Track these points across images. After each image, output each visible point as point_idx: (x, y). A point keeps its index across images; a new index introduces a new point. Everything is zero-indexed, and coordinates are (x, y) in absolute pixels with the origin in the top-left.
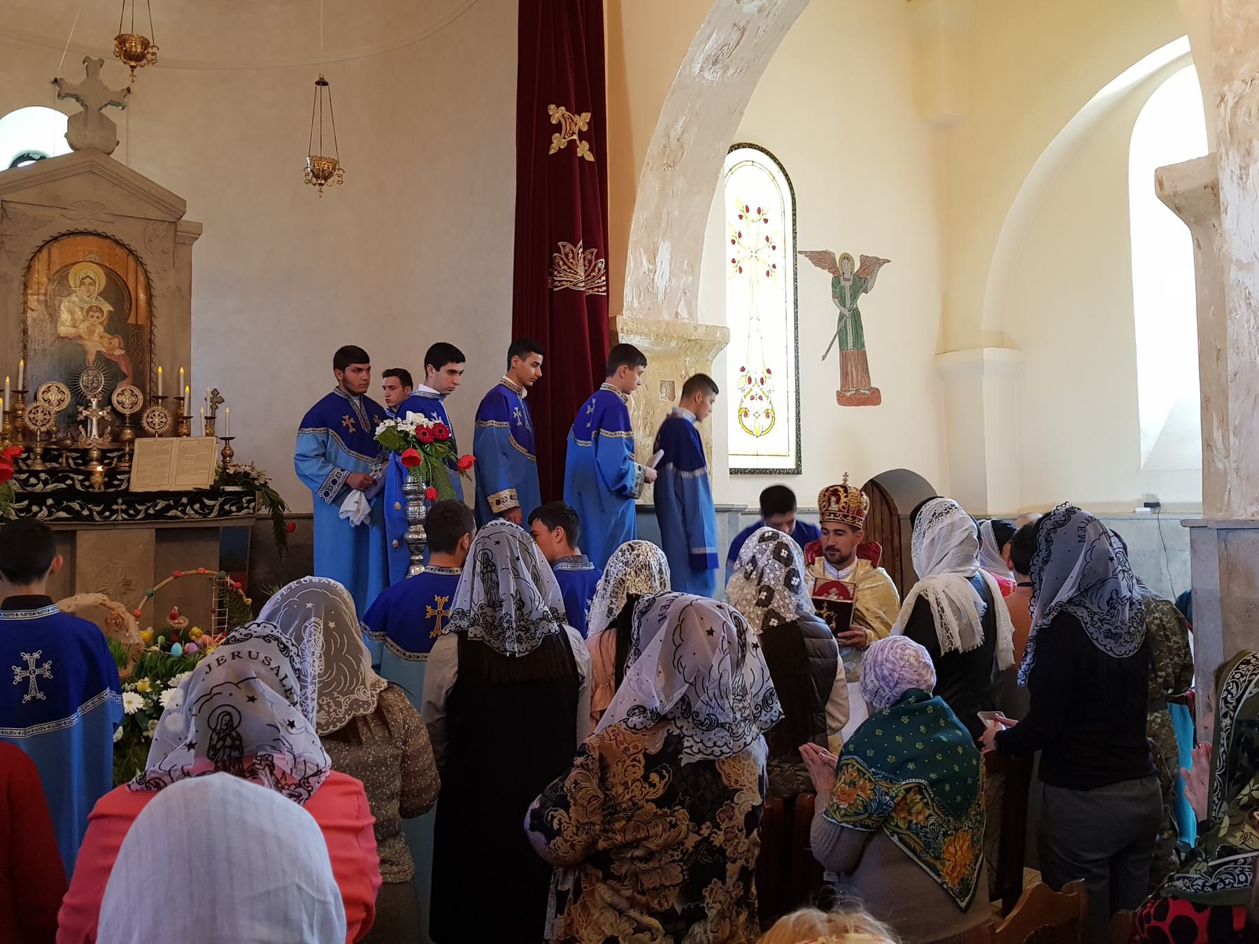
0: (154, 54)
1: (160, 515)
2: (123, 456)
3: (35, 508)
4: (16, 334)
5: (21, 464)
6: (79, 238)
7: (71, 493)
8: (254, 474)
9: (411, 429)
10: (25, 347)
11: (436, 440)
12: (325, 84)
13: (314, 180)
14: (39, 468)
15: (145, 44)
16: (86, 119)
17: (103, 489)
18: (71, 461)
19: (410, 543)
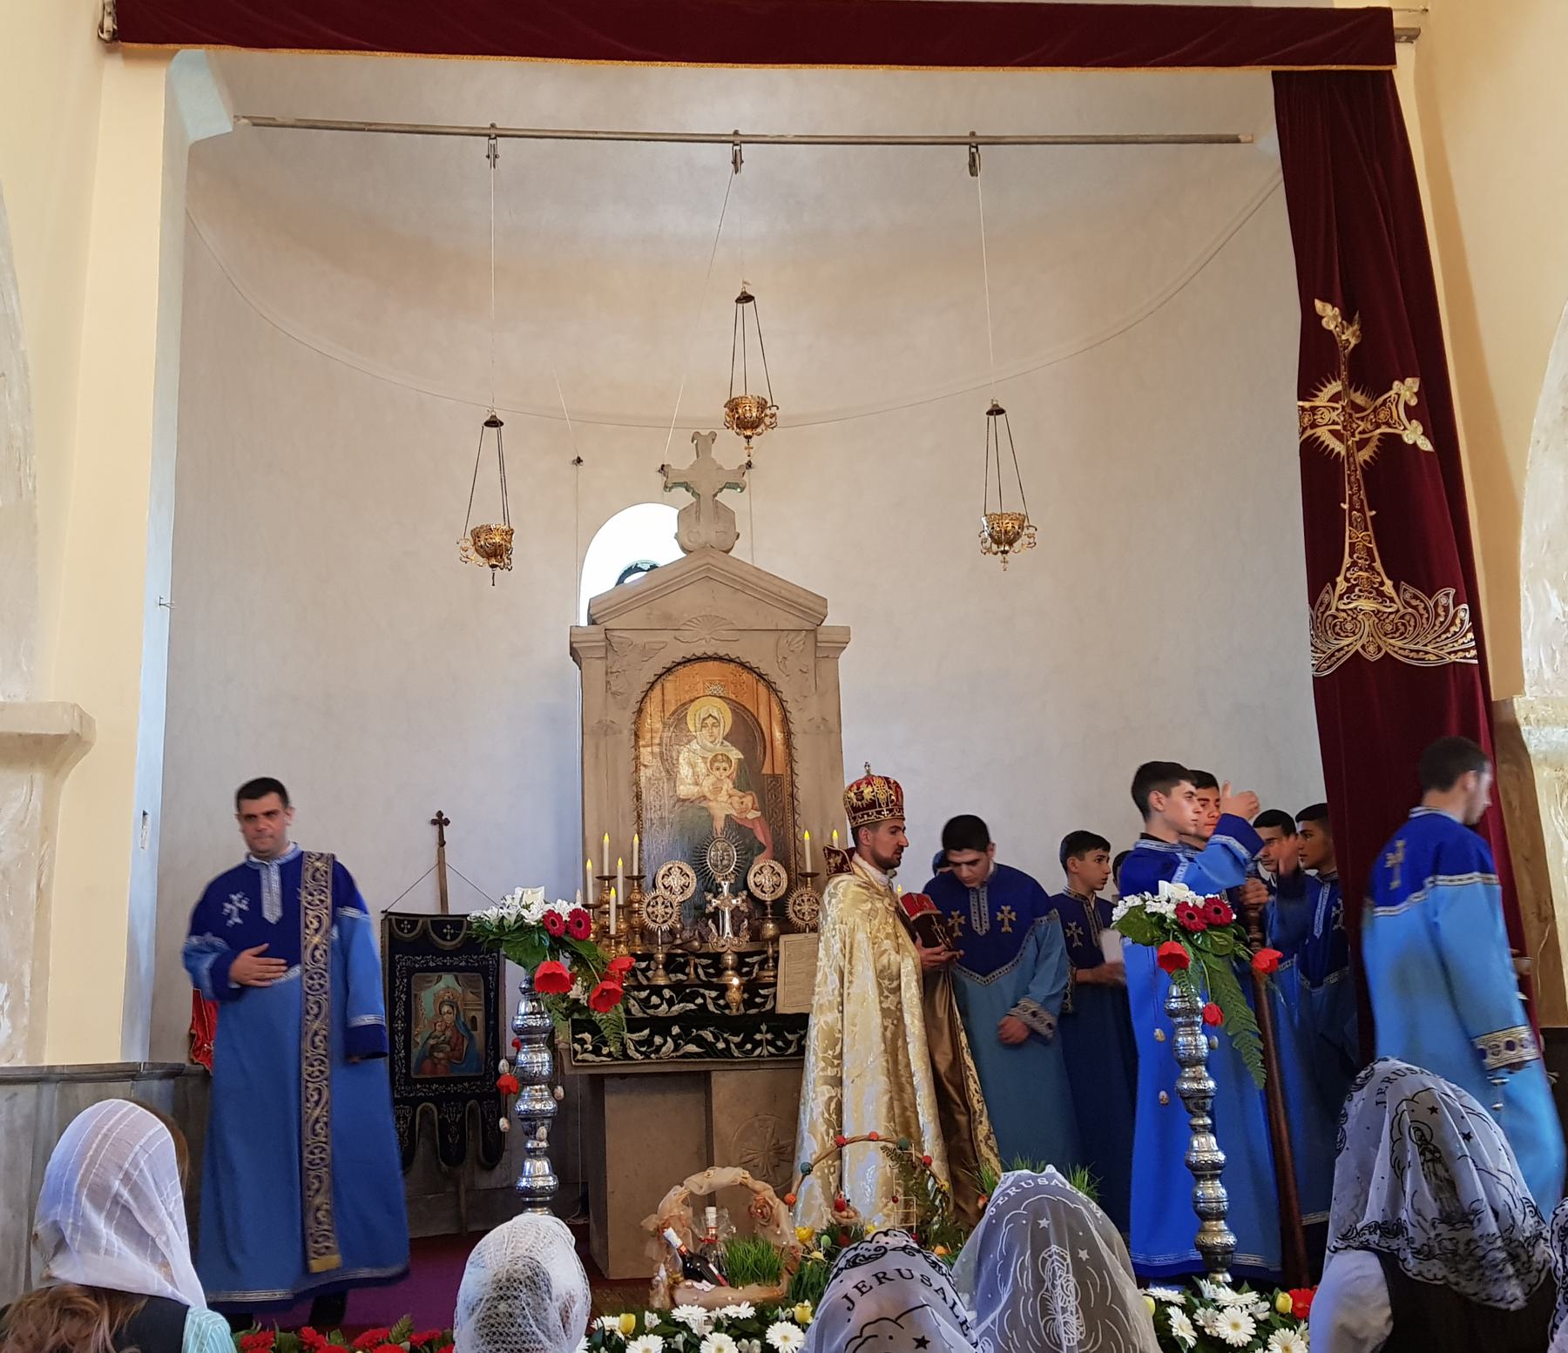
0: (773, 416)
2: (765, 961)
3: (658, 1040)
4: (628, 802)
7: (701, 1018)
10: (639, 816)
12: (1001, 412)
14: (661, 982)
15: (762, 405)
16: (698, 512)
18: (700, 971)
19: (1187, 1097)
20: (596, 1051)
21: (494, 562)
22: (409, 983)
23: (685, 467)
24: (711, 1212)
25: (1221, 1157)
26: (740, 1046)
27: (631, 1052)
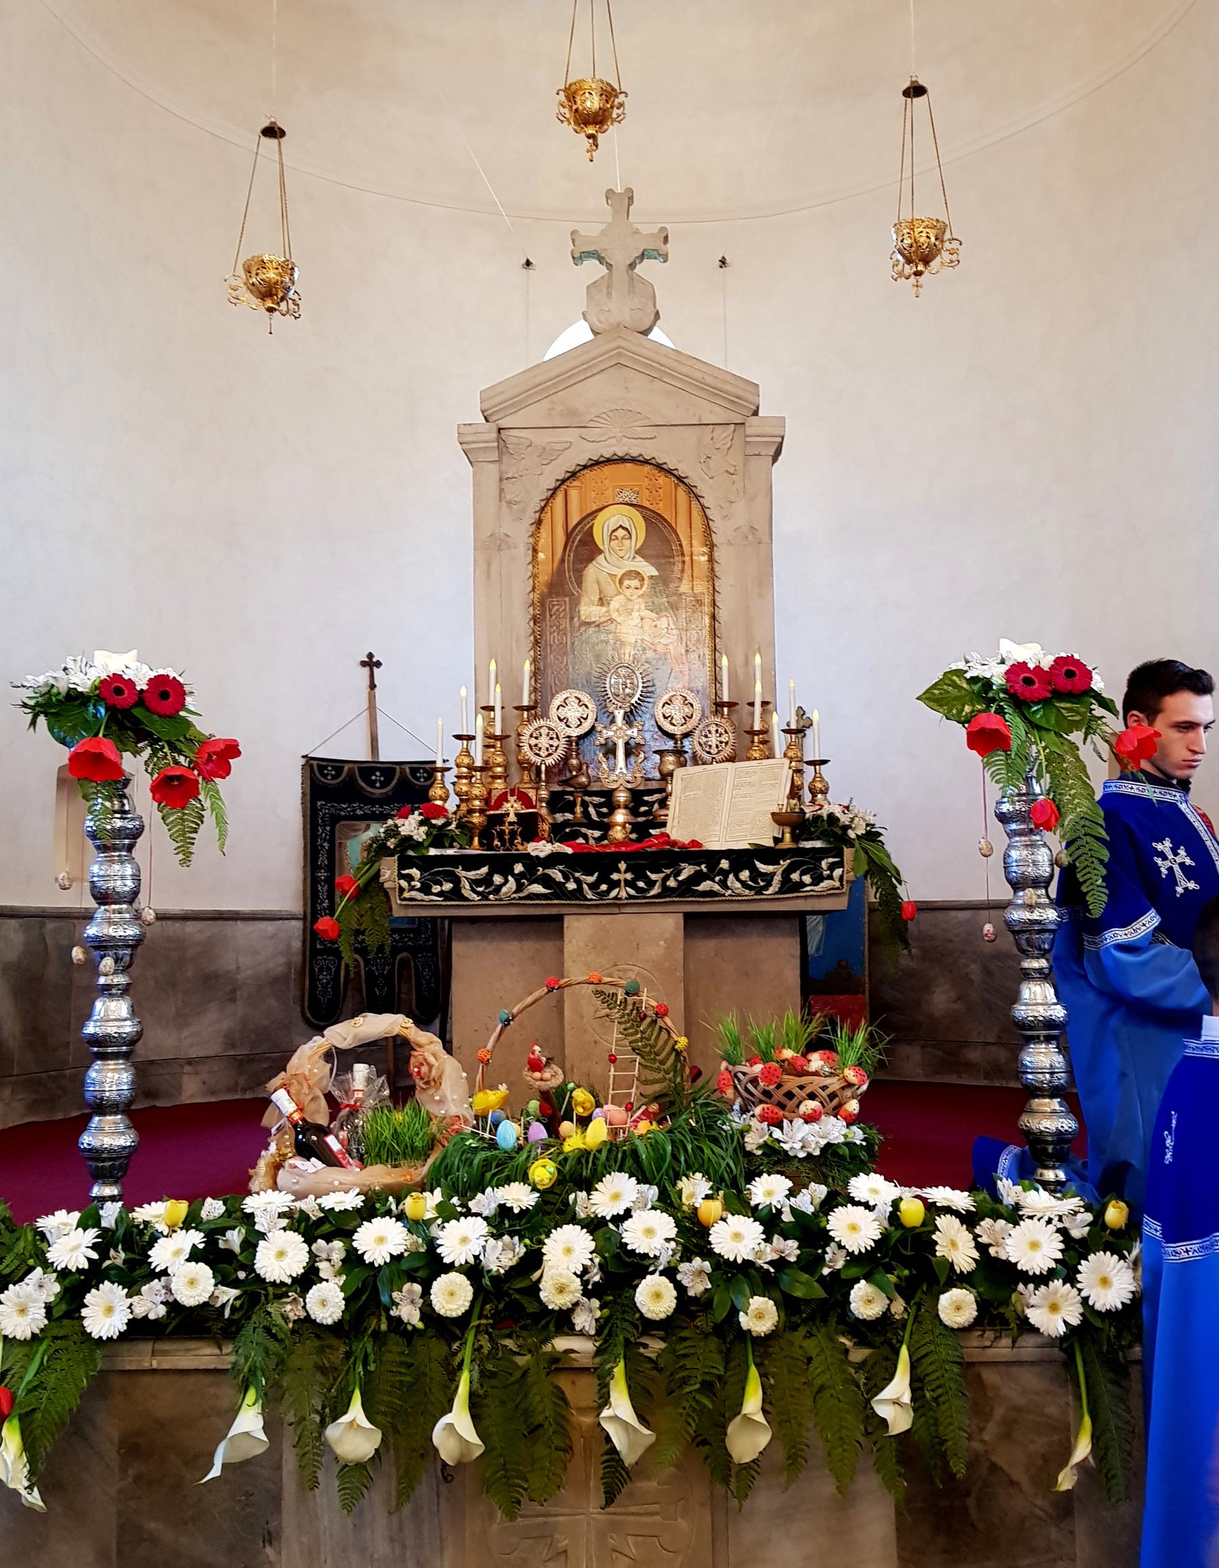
0: (621, 105)
1: (686, 888)
3: (498, 879)
6: (607, 470)
8: (844, 819)
9: (996, 673)
11: (1060, 695)
13: (908, 269)
15: (609, 93)
19: (1016, 930)
20: (425, 889)
22: (332, 832)
24: (361, 1071)
25: (1059, 1012)
27: (466, 891)
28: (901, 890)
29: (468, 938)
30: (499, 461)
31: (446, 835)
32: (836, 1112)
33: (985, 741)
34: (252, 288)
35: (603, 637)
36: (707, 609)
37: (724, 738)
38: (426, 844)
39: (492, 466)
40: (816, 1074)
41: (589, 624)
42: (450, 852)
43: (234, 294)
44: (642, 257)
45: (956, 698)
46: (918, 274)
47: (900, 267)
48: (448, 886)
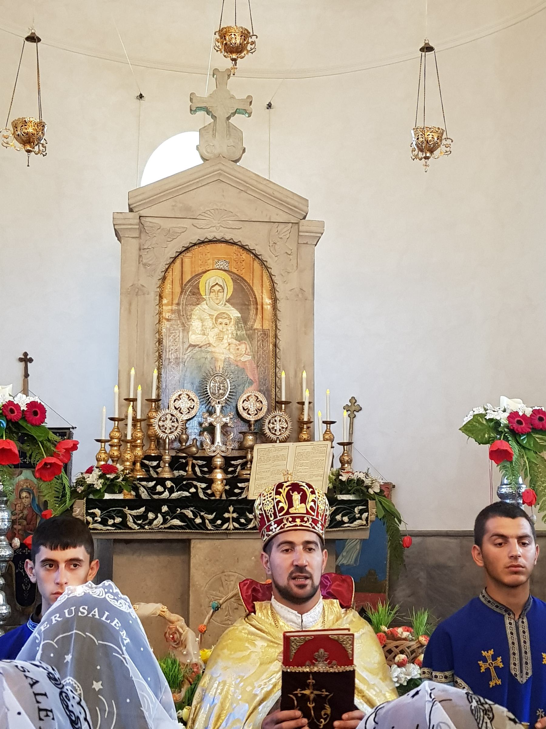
0: (253, 43)
2: (246, 463)
3: (151, 515)
4: (152, 345)
5: (152, 472)
6: (209, 247)
7: (193, 501)
8: (367, 482)
9: (503, 418)
10: (160, 356)
11: (536, 430)
13: (421, 155)
14: (167, 475)
15: (246, 35)
16: (214, 130)
17: (224, 497)
18: (197, 469)
20: (104, 522)
21: (29, 148)
23: (206, 95)
26: (212, 521)
27: (130, 523)
28: (402, 527)
29: (122, 553)
30: (139, 237)
31: (116, 485)
32: (413, 661)
33: (499, 456)
34: (17, 137)
35: (203, 354)
36: (271, 340)
37: (285, 425)
38: (102, 491)
39: (134, 240)
40: (405, 639)
41: (195, 346)
42: (120, 497)
43: (5, 140)
44: (234, 114)
45: (480, 430)
46: (427, 158)
47: (416, 152)
48: (118, 520)
